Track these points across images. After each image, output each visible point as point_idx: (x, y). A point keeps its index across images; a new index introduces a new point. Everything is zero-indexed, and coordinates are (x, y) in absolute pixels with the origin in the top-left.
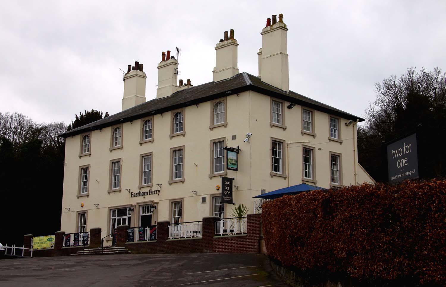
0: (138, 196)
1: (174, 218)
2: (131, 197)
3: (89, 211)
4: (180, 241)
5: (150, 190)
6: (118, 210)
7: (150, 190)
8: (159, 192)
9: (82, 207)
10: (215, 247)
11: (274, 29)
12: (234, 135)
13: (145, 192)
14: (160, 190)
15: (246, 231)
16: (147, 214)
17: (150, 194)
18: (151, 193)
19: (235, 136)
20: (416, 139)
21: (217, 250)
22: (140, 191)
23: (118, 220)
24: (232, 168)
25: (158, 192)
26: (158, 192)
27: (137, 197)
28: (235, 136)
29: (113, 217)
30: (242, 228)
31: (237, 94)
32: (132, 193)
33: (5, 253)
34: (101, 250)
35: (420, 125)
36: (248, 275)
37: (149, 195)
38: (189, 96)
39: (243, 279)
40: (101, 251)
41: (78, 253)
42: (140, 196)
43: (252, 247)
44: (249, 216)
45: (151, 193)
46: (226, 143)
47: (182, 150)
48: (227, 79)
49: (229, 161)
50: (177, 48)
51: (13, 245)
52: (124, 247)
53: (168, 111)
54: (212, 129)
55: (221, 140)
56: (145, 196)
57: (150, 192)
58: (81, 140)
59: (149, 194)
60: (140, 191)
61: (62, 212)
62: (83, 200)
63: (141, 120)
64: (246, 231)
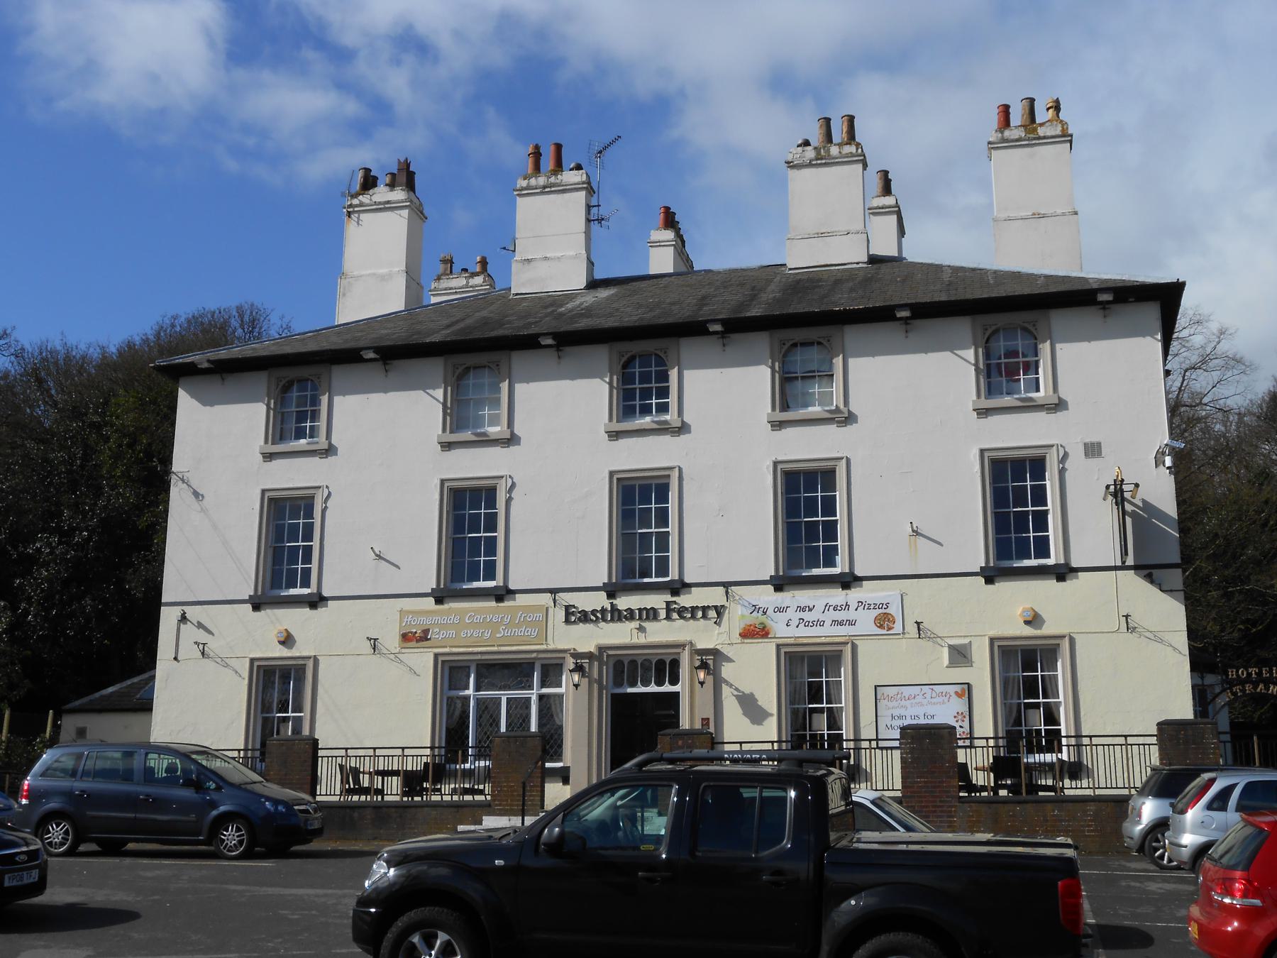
0: (604, 620)
5: (668, 603)
7: (668, 603)
11: (1045, 138)
12: (1094, 439)
13: (640, 610)
16: (653, 688)
17: (668, 618)
20: (442, 933)
25: (712, 614)
27: (602, 624)
31: (385, 364)
35: (703, 785)
39: (1242, 828)
42: (612, 620)
45: (675, 616)
48: (845, 264)
53: (964, 314)
56: (646, 624)
59: (663, 614)
61: (158, 658)
64: (1006, 791)
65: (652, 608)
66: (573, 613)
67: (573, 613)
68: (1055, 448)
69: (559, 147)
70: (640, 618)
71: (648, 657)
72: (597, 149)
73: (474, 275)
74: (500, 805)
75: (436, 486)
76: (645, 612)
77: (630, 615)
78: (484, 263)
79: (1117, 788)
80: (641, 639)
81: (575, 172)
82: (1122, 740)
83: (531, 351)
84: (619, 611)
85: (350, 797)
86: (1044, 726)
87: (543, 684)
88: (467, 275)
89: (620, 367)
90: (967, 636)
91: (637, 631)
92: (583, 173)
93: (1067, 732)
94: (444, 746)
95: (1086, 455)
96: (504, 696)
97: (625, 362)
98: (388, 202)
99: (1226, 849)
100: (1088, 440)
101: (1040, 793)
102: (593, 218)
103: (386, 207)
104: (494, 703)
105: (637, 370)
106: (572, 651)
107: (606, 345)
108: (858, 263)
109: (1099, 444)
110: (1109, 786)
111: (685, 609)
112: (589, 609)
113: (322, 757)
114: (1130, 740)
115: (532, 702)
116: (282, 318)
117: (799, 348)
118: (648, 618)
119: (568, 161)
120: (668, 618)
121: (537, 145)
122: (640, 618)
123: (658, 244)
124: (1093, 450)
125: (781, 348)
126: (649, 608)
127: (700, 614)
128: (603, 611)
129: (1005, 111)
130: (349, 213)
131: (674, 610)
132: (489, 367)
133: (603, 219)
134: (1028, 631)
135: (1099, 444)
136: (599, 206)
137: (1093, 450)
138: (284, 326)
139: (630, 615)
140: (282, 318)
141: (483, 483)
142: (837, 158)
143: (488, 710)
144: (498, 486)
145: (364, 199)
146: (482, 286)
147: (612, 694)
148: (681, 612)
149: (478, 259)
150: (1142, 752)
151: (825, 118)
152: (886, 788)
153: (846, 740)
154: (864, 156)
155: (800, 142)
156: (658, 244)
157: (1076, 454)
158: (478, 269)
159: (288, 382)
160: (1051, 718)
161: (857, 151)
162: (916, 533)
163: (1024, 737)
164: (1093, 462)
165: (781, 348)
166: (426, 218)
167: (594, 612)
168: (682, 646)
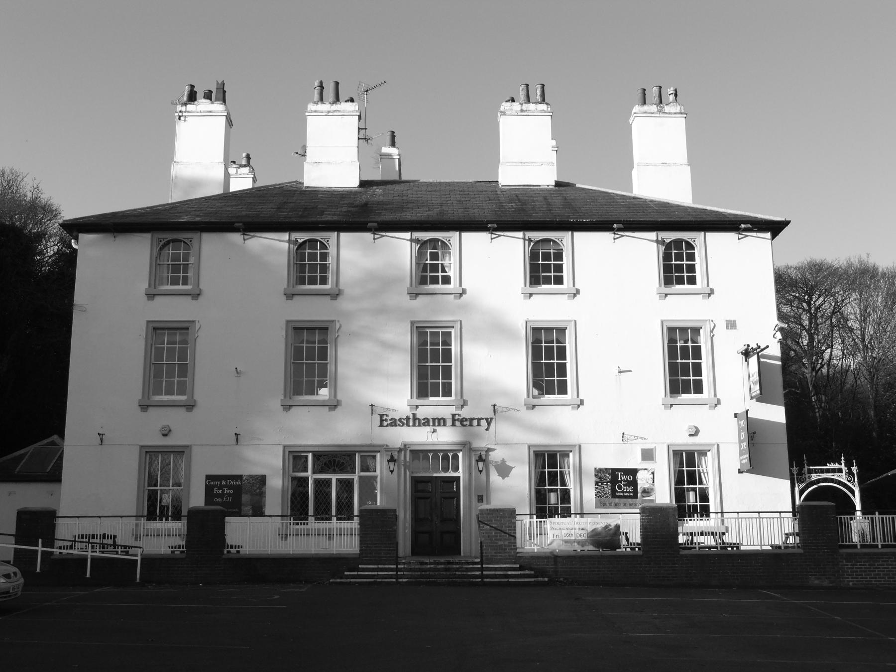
0: (408, 425)
1: (147, 491)
2: (381, 425)
3: (194, 448)
4: (882, 554)
5: (453, 415)
7: (453, 415)
8: (489, 423)
9: (165, 435)
10: (845, 574)
11: (670, 114)
14: (492, 419)
15: (639, 541)
17: (453, 425)
18: (457, 423)
19: (735, 328)
21: (852, 581)
23: (317, 482)
25: (484, 423)
26: (484, 423)
27: (405, 427)
28: (735, 328)
32: (385, 417)
33: (86, 575)
38: (704, 216)
40: (478, 573)
41: (348, 577)
42: (414, 425)
43: (850, 577)
45: (457, 423)
46: (196, 335)
47: (187, 329)
52: (518, 566)
54: (292, 297)
55: (185, 325)
59: (449, 422)
62: (159, 418)
63: (152, 237)
65: (442, 418)
66: (386, 420)
67: (386, 420)
68: (708, 322)
69: (337, 84)
70: (434, 425)
72: (363, 88)
73: (241, 166)
76: (442, 420)
77: (426, 422)
78: (248, 157)
79: (754, 545)
81: (350, 103)
82: (777, 515)
84: (419, 420)
86: (700, 502)
87: (365, 468)
88: (236, 166)
91: (431, 433)
92: (356, 105)
93: (575, 511)
95: (727, 328)
96: (334, 477)
100: (728, 319)
101: (617, 550)
102: (229, 122)
103: (210, 114)
104: (341, 483)
105: (552, 262)
106: (385, 447)
110: (749, 544)
112: (397, 418)
113: (728, 518)
114: (762, 515)
116: (34, 180)
117: (540, 243)
118: (439, 425)
120: (453, 425)
121: (321, 81)
122: (434, 425)
123: (387, 157)
124: (731, 325)
126: (440, 418)
127: (468, 423)
130: (180, 117)
133: (370, 139)
136: (366, 129)
137: (731, 325)
138: (35, 186)
140: (34, 180)
143: (322, 486)
145: (190, 107)
149: (244, 155)
150: (769, 522)
152: (749, 544)
153: (145, 516)
155: (508, 99)
156: (387, 157)
158: (244, 162)
159: (167, 242)
160: (704, 497)
161: (547, 110)
166: (232, 125)
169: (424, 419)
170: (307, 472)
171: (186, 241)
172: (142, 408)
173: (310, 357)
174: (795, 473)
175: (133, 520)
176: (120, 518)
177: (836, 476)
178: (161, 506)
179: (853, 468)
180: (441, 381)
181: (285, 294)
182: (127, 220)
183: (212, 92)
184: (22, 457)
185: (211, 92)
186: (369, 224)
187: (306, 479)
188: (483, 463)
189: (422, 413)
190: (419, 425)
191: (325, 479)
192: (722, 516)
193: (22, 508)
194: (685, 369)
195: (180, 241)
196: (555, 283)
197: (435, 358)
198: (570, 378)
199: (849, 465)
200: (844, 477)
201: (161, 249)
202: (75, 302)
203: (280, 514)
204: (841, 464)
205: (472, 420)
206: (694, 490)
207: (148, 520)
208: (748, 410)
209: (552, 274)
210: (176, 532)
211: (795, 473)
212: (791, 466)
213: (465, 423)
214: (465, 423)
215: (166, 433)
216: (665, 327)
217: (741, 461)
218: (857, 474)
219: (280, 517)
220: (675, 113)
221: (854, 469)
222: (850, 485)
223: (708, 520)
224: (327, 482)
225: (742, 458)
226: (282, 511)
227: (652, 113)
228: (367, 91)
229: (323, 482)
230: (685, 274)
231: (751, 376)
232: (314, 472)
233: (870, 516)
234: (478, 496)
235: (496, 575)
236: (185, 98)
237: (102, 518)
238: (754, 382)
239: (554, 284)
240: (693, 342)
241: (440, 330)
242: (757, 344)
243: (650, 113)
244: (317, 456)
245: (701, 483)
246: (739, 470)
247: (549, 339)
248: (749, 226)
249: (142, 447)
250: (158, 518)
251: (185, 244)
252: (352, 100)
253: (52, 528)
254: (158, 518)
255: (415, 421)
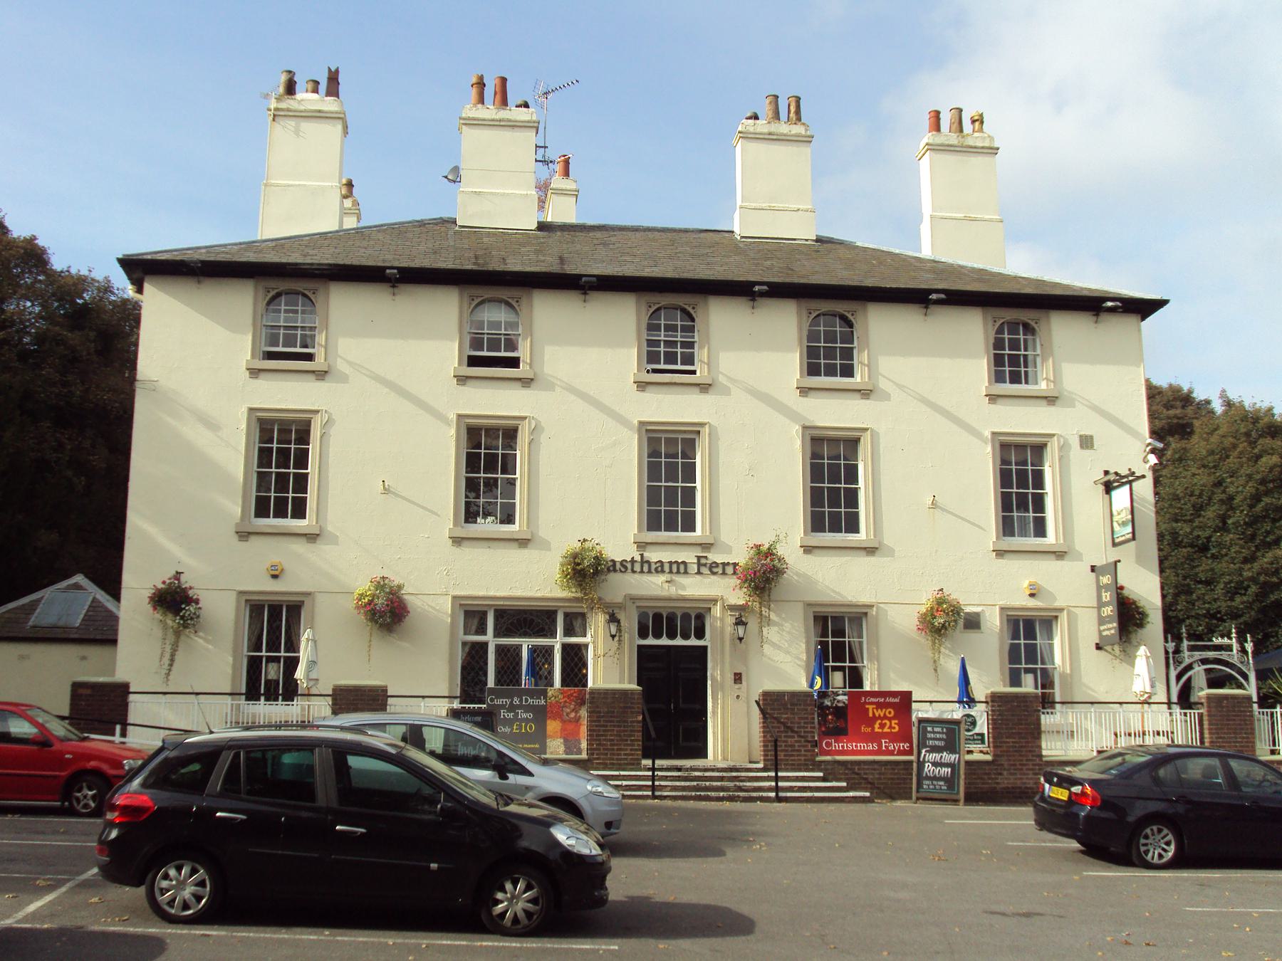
6: (496, 611)
7: (699, 558)
9: (275, 577)
11: (975, 147)
13: (671, 563)
22: (642, 555)
23: (500, 650)
24: (1123, 538)
29: (465, 634)
30: (1146, 724)
34: (769, 789)
36: (26, 772)
37: (698, 577)
44: (130, 315)
45: (705, 570)
48: (795, 240)
49: (1115, 519)
50: (1143, 308)
51: (118, 728)
57: (699, 564)
58: (255, 304)
60: (642, 555)
62: (265, 553)
68: (1055, 438)
70: (671, 572)
71: (686, 611)
72: (541, 89)
74: (598, 759)
75: (243, 412)
77: (660, 568)
80: (672, 591)
81: (523, 109)
83: (891, 304)
85: (1053, 743)
87: (569, 631)
89: (994, 333)
90: (980, 605)
94: (459, 695)
95: (1082, 447)
97: (847, 317)
98: (320, 111)
99: (934, 802)
100: (1082, 433)
107: (252, 280)
108: (807, 240)
109: (1091, 437)
111: (717, 565)
112: (618, 559)
115: (556, 651)
118: (678, 572)
119: (513, 98)
120: (699, 573)
122: (671, 572)
125: (470, 304)
126: (680, 561)
127: (720, 570)
128: (633, 561)
129: (936, 116)
131: (705, 565)
132: (305, 295)
134: (1032, 603)
135: (1091, 437)
136: (545, 147)
139: (660, 568)
141: (298, 415)
142: (956, 146)
143: (508, 657)
144: (520, 427)
146: (350, 209)
147: (638, 646)
148: (713, 567)
151: (774, 96)
153: (242, 694)
154: (344, 114)
155: (749, 115)
157: (1075, 443)
162: (387, 490)
163: (263, 695)
164: (1087, 452)
165: (470, 304)
167: (623, 563)
168: (715, 601)
169: (656, 563)
170: (486, 635)
171: (306, 292)
172: (240, 536)
173: (672, 476)
174: (1170, 650)
175: (228, 699)
176: (193, 696)
177: (1224, 655)
178: (267, 682)
179: (1246, 644)
180: (680, 509)
181: (248, 369)
182: (221, 258)
183: (318, 83)
184: (39, 601)
185: (317, 83)
186: (584, 279)
187: (484, 646)
188: (616, 624)
189: (653, 556)
190: (650, 572)
191: (543, 647)
192: (1169, 708)
193: (1002, 674)
194: (834, 494)
195: (297, 293)
196: (826, 375)
197: (835, 478)
198: (311, 496)
199: (1242, 640)
200: (1236, 657)
201: (269, 303)
202: (139, 377)
203: (447, 695)
204: (1230, 638)
205: (724, 565)
206: (1033, 671)
207: (248, 699)
208: (1119, 561)
209: (838, 362)
210: (248, 718)
211: (1170, 650)
212: (1166, 640)
213: (715, 570)
214: (715, 570)
215: (276, 573)
216: (517, 422)
217: (1100, 632)
218: (1253, 652)
219: (447, 699)
220: (983, 148)
221: (1249, 647)
222: (1244, 669)
223: (1052, 713)
224: (546, 651)
225: (1102, 628)
226: (451, 689)
227: (951, 146)
228: (546, 93)
229: (509, 650)
230: (822, 361)
231: (1115, 513)
232: (497, 634)
233: (1269, 710)
234: (735, 674)
235: (811, 792)
236: (281, 90)
237: (426, 699)
238: (1120, 522)
239: (825, 375)
240: (684, 456)
241: (663, 436)
242: (1130, 469)
243: (948, 146)
244: (501, 614)
245: (852, 660)
246: (1097, 644)
247: (671, 451)
248: (943, 296)
249: (241, 593)
250: (280, 697)
251: (305, 299)
252: (526, 105)
253: (124, 707)
254: (280, 697)
255: (647, 567)
